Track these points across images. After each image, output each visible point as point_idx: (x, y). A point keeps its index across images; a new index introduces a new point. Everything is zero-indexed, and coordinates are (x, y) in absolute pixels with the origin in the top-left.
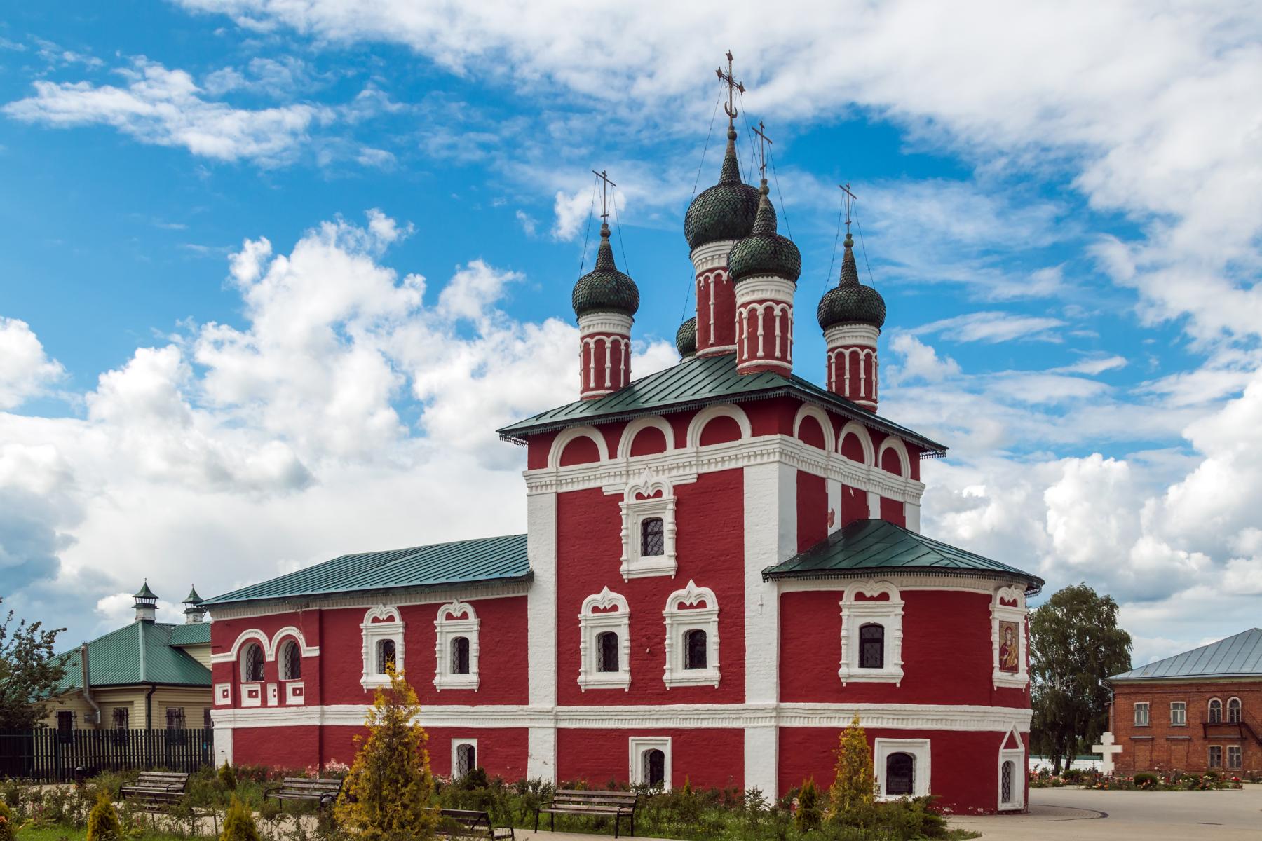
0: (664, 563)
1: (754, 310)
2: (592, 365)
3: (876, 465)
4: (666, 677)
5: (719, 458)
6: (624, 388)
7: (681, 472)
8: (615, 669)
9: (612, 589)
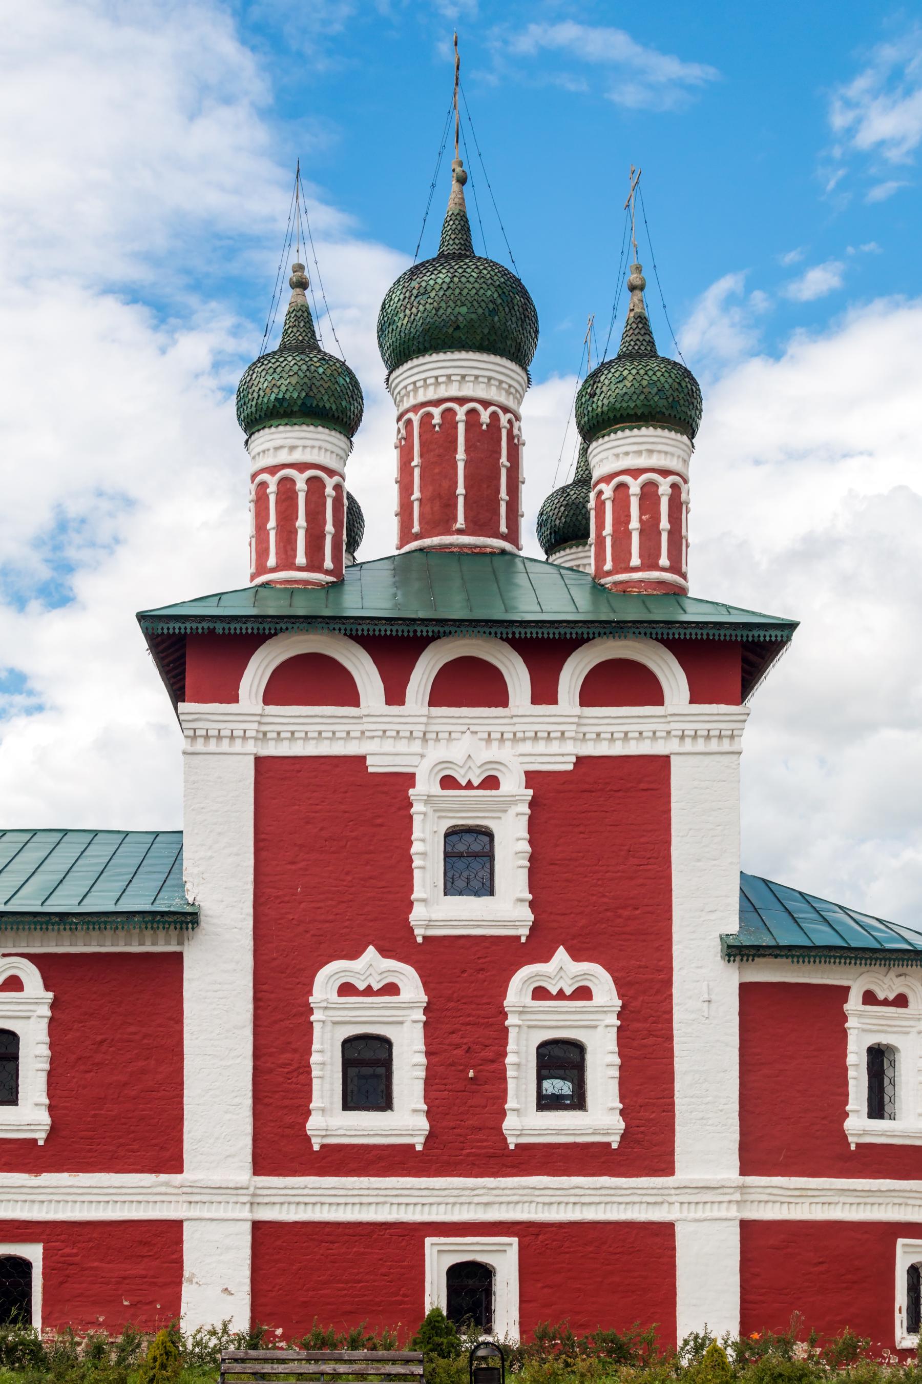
0: (506, 908)
2: (272, 523)
5: (620, 732)
7: (541, 747)
8: (384, 1102)
9: (385, 952)
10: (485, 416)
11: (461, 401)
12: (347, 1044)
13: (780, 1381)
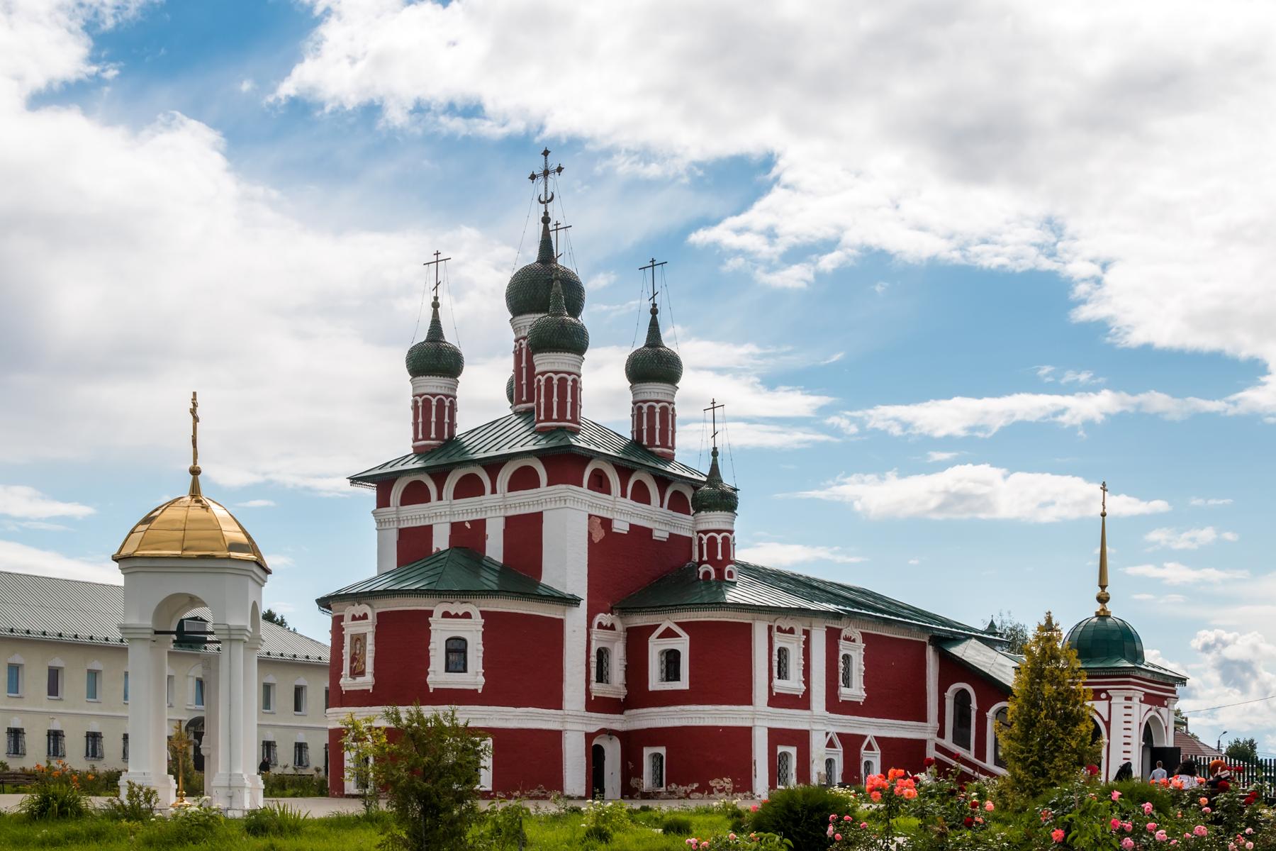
1: (566, 380)
2: (420, 420)
3: (661, 506)
5: (524, 502)
6: (451, 443)
13: (1099, 850)
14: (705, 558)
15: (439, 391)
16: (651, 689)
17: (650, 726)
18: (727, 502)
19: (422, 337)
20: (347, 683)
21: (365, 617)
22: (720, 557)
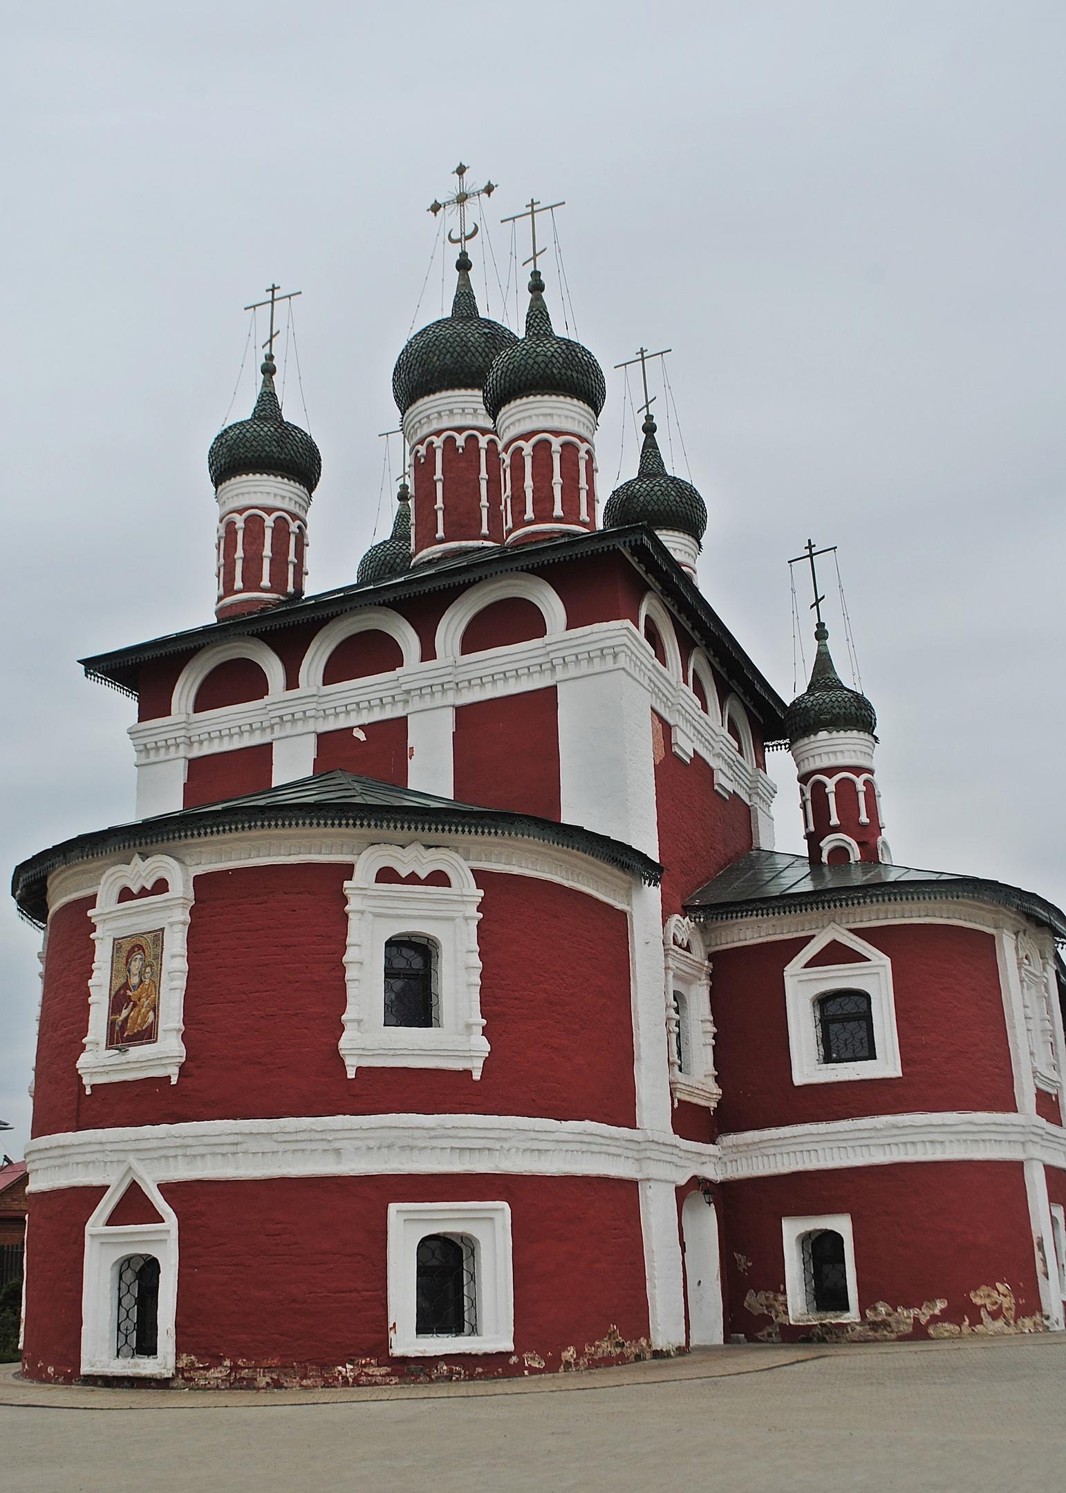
2: (240, 553)
4: (345, 1043)
5: (506, 671)
10: (460, 440)
11: (460, 430)
12: (425, 1242)
14: (835, 821)
15: (278, 503)
16: (799, 1079)
17: (800, 1167)
18: (857, 716)
19: (245, 412)
20: (97, 1063)
21: (161, 886)
22: (864, 819)
